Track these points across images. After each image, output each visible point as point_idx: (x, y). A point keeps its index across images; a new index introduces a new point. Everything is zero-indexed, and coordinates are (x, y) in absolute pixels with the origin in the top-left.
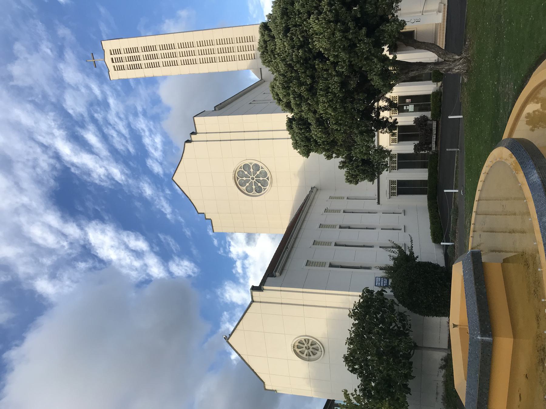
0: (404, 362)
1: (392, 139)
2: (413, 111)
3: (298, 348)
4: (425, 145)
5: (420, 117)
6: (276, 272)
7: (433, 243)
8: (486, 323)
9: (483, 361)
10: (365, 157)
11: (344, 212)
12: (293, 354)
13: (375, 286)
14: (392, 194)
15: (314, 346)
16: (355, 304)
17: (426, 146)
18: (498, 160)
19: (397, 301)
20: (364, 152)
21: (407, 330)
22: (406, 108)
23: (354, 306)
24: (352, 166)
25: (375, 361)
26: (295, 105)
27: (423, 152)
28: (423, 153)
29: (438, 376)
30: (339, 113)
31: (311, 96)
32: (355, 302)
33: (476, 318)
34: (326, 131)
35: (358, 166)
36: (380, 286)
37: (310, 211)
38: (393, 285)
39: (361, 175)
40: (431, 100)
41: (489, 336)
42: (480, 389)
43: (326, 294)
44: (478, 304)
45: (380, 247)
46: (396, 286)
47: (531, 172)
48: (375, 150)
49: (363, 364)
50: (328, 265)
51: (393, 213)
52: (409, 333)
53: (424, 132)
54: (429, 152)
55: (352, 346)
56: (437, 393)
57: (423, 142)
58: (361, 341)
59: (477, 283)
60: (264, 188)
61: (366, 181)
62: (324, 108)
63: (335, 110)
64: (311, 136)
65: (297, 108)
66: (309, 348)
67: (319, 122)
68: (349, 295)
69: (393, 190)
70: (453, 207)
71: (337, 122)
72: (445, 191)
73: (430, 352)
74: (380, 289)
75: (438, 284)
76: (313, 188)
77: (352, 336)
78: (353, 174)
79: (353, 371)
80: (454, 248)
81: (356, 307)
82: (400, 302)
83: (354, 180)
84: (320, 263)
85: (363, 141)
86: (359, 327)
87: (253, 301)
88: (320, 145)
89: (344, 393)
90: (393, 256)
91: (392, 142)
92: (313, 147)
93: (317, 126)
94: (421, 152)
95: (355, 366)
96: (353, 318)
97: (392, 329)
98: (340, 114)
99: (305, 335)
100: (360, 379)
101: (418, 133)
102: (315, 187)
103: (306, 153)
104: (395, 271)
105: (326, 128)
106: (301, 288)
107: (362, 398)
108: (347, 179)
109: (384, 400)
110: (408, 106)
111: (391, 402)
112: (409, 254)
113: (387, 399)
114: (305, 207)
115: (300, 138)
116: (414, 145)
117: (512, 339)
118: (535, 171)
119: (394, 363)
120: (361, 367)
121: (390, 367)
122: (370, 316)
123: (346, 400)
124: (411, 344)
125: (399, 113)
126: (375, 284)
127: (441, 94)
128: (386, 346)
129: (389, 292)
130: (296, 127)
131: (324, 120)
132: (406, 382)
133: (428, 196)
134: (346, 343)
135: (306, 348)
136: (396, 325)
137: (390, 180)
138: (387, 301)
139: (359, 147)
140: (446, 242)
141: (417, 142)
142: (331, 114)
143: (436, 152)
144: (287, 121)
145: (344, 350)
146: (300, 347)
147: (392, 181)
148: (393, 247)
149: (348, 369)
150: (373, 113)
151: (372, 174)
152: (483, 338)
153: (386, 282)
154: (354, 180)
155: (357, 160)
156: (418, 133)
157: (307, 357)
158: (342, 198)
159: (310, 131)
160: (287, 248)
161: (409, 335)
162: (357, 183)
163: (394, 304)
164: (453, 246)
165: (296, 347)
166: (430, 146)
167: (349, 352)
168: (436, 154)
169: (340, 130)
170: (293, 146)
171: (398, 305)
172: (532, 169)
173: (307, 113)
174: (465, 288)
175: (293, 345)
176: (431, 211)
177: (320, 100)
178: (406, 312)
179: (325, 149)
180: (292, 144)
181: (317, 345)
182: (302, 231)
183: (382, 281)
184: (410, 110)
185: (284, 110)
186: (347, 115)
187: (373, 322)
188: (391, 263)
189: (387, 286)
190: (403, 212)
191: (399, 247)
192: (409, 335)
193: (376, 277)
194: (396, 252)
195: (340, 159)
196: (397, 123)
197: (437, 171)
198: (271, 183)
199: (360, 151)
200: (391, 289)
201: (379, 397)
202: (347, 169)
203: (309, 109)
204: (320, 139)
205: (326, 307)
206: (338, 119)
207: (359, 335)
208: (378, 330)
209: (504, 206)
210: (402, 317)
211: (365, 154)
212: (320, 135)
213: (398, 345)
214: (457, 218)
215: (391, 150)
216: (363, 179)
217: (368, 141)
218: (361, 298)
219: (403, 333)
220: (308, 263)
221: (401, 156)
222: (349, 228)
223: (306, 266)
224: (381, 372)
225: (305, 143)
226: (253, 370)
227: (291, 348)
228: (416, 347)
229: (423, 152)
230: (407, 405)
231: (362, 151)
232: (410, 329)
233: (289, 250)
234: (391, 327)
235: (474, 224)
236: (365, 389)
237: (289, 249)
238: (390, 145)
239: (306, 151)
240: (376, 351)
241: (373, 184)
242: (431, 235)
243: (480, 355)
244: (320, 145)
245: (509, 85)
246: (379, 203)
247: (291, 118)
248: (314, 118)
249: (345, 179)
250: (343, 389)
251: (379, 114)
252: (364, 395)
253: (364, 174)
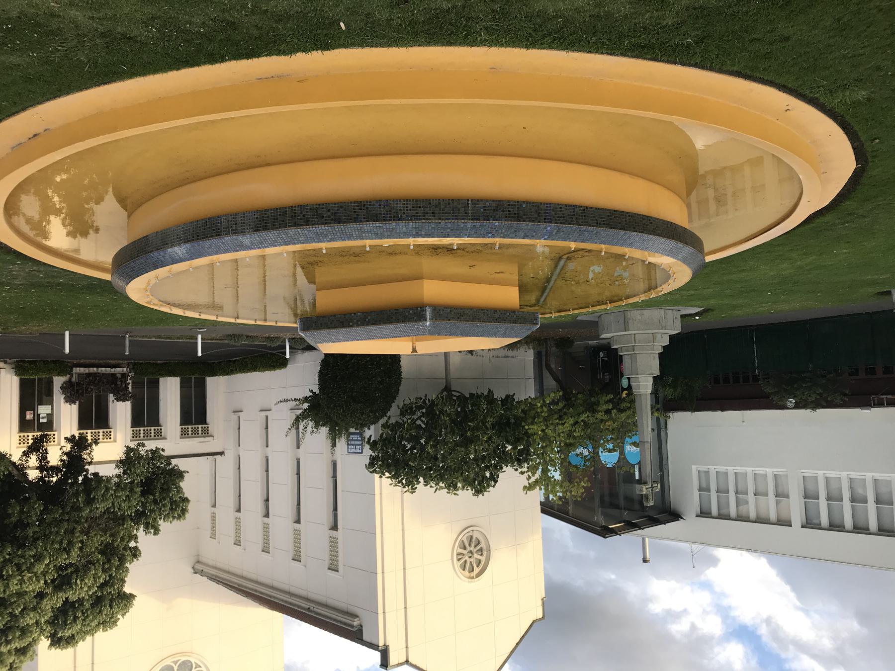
0: (471, 405)
1: (103, 439)
2: (50, 406)
3: (473, 571)
4: (116, 384)
5: (63, 394)
6: (352, 626)
7: (287, 368)
8: (407, 314)
9: (458, 318)
10: (138, 490)
11: (239, 510)
12: (482, 578)
13: (362, 453)
14: (206, 433)
15: (467, 545)
16: (393, 484)
17: (119, 383)
18: (148, 293)
19: (383, 419)
20: (128, 493)
21: (424, 402)
22: (43, 418)
23: (397, 486)
24: (154, 511)
25: (475, 448)
26: (22, 639)
27: (130, 386)
28: (132, 386)
29: (483, 356)
30: (46, 549)
31: (6, 608)
32: (391, 484)
33: (401, 326)
34: (81, 570)
35: (155, 502)
36: (362, 445)
37: (239, 572)
38: (358, 427)
39: (171, 495)
40: (32, 377)
41: (423, 310)
42: (497, 320)
43: (382, 533)
44: (380, 324)
45: (297, 448)
46: (361, 422)
47: (170, 255)
48: (124, 475)
49: (483, 465)
50: (333, 533)
51: (239, 428)
52: (429, 399)
53: (93, 387)
54: (129, 378)
55: (459, 485)
56: (506, 357)
57: (112, 388)
58: (449, 472)
59: (349, 324)
60: (196, 668)
61: (182, 484)
62: (34, 579)
63: (38, 558)
64: (91, 596)
65: (29, 635)
66: (471, 552)
67: (63, 585)
68: (381, 494)
69: (198, 431)
70: (226, 342)
71: (65, 549)
72: (200, 354)
73: (452, 368)
74: (367, 447)
75: (353, 361)
76: (194, 570)
77: (443, 485)
78: (169, 509)
79: (494, 479)
80: (294, 338)
81: (398, 483)
82: (384, 414)
83: (181, 505)
84: (331, 546)
85: (106, 497)
86: (428, 475)
87: (407, 662)
88: (110, 576)
89: (528, 491)
90: (312, 428)
91: (110, 438)
92: (114, 590)
93: (70, 587)
94: (130, 389)
95: (487, 477)
96: (416, 486)
97: (426, 424)
98: (49, 546)
99: (451, 561)
100: (505, 468)
101: (94, 396)
102: (192, 566)
103: (127, 599)
104: (337, 424)
105: (77, 571)
106: (377, 576)
107: (530, 463)
108: (179, 517)
109: (528, 431)
110: (41, 416)
111: (530, 421)
112: (307, 404)
113: (526, 427)
114: (231, 582)
115: (95, 618)
116: (117, 401)
117: (425, 281)
118: (170, 250)
119: (475, 420)
120: (487, 467)
121: (481, 424)
122: (409, 460)
123: (538, 487)
124: (445, 397)
125: (54, 429)
126: (359, 453)
127: (21, 361)
128: (452, 433)
129: (371, 432)
130: (69, 629)
131: (59, 575)
132: (499, 401)
133: (209, 376)
134: (455, 494)
135: (470, 557)
136: (419, 418)
137: (181, 438)
138: (384, 434)
139: (118, 503)
140: (285, 349)
141: (111, 397)
142: (48, 565)
143: (131, 366)
144: (56, 649)
145: (466, 494)
146: (471, 568)
147: (182, 435)
148: (298, 428)
149: (494, 486)
150: (51, 479)
151: (170, 476)
152: (428, 319)
153: (355, 437)
154: (181, 505)
155: (142, 503)
156: (94, 396)
157: (485, 553)
158: (213, 516)
159: (81, 601)
160: (309, 608)
161: (432, 400)
162: (186, 500)
163: (389, 424)
164: (291, 340)
165: (472, 574)
166: (119, 376)
167: (467, 487)
168: (135, 366)
169: (82, 542)
170: (110, 628)
171: (389, 417)
172: (166, 254)
173: (43, 613)
174: (358, 340)
175: (470, 580)
176: (235, 372)
177: (16, 590)
178: (398, 406)
179: (118, 565)
180: (107, 630)
181: (465, 539)
182: (276, 584)
183: (353, 442)
184: (49, 412)
185: (31, 656)
186: (51, 532)
187: (418, 455)
188: (324, 430)
189: (361, 434)
190: (235, 413)
191: (297, 419)
192: (432, 400)
193: (348, 453)
194: (305, 423)
195: (141, 533)
196: (73, 436)
197: (164, 363)
198: (184, 654)
199: (125, 501)
200: (366, 429)
201: (526, 438)
202: (160, 519)
203: (34, 609)
204: (99, 578)
205: (403, 530)
206: (60, 549)
207: (440, 475)
208: (430, 447)
209: (226, 286)
210: (407, 411)
211: (131, 490)
212: (89, 580)
213: (448, 415)
214: (246, 336)
215: (126, 446)
216: (179, 490)
217: (107, 489)
218: (384, 475)
219: (431, 409)
220: (334, 568)
221: (137, 420)
222: (267, 500)
223: (338, 571)
224: (489, 439)
225: (105, 606)
226: (517, 644)
227: (474, 582)
228: (447, 388)
229: (130, 386)
230: (530, 399)
231: (127, 496)
232: (424, 398)
233: (311, 606)
234: (424, 426)
235: (256, 320)
236: (519, 459)
237: (311, 605)
238: (115, 441)
239: (122, 602)
240: (462, 446)
241: (188, 472)
242: (275, 370)
243: (451, 321)
244: (110, 576)
245: (14, 271)
246: (221, 453)
247: (49, 642)
248: (54, 596)
249: (179, 521)
250: (522, 493)
251: (55, 469)
252: (526, 460)
253: (169, 490)
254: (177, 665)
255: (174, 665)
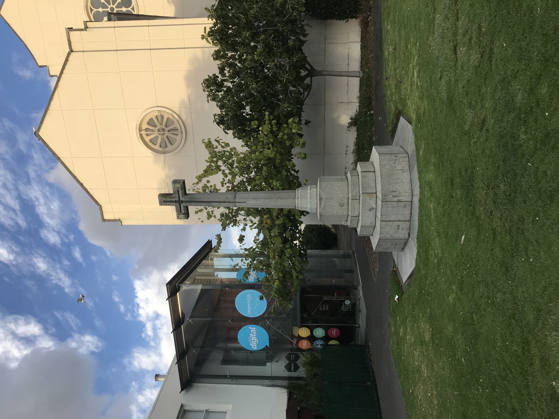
226: (82, 185)
227: (137, 132)
254: (131, 10)
255: (131, 7)
